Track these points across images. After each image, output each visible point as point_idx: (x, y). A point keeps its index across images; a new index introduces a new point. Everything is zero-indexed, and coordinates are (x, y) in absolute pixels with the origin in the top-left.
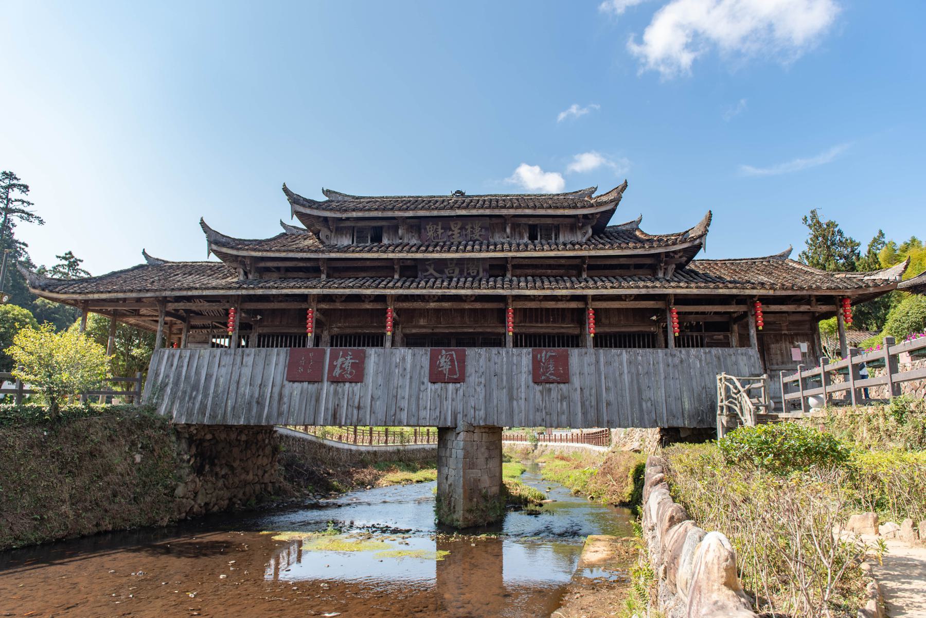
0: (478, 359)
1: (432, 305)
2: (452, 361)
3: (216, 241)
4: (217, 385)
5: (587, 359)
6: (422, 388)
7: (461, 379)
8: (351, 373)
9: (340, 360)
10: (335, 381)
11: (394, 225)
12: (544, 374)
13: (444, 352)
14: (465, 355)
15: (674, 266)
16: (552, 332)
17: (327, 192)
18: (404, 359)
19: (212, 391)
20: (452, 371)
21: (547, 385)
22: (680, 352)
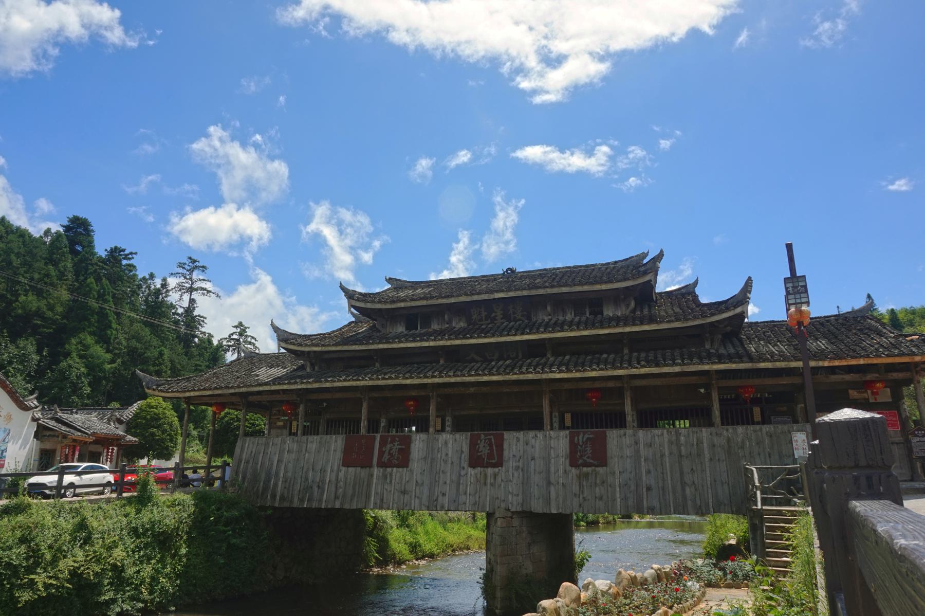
0: (515, 443)
1: (472, 390)
2: (491, 445)
3: (284, 337)
4: (286, 472)
5: (627, 441)
6: (463, 473)
7: (499, 464)
8: (398, 458)
9: (389, 446)
10: (381, 464)
11: (439, 311)
12: (581, 456)
13: (483, 436)
14: (503, 439)
15: (720, 336)
16: (592, 415)
17: (390, 280)
18: (446, 443)
19: (282, 475)
20: (490, 456)
21: (585, 469)
22: (727, 430)
